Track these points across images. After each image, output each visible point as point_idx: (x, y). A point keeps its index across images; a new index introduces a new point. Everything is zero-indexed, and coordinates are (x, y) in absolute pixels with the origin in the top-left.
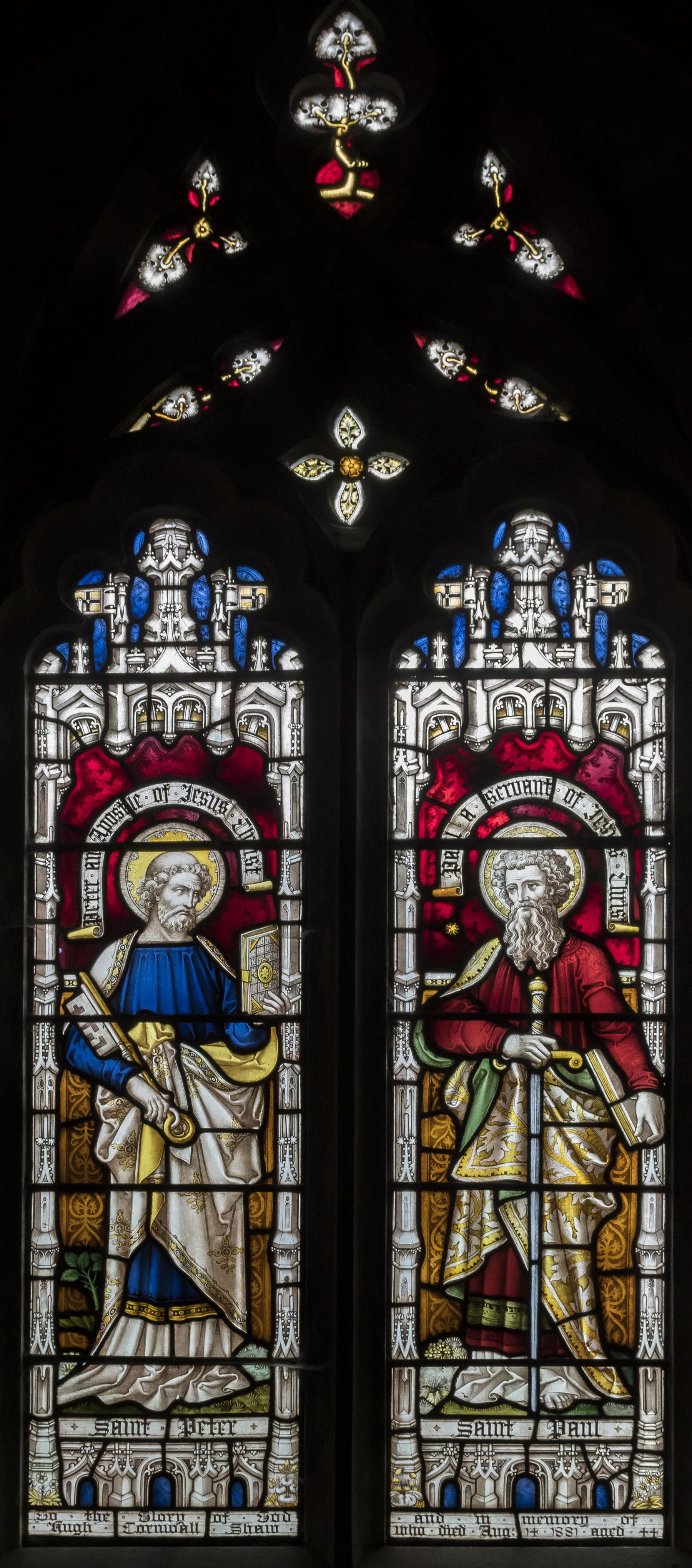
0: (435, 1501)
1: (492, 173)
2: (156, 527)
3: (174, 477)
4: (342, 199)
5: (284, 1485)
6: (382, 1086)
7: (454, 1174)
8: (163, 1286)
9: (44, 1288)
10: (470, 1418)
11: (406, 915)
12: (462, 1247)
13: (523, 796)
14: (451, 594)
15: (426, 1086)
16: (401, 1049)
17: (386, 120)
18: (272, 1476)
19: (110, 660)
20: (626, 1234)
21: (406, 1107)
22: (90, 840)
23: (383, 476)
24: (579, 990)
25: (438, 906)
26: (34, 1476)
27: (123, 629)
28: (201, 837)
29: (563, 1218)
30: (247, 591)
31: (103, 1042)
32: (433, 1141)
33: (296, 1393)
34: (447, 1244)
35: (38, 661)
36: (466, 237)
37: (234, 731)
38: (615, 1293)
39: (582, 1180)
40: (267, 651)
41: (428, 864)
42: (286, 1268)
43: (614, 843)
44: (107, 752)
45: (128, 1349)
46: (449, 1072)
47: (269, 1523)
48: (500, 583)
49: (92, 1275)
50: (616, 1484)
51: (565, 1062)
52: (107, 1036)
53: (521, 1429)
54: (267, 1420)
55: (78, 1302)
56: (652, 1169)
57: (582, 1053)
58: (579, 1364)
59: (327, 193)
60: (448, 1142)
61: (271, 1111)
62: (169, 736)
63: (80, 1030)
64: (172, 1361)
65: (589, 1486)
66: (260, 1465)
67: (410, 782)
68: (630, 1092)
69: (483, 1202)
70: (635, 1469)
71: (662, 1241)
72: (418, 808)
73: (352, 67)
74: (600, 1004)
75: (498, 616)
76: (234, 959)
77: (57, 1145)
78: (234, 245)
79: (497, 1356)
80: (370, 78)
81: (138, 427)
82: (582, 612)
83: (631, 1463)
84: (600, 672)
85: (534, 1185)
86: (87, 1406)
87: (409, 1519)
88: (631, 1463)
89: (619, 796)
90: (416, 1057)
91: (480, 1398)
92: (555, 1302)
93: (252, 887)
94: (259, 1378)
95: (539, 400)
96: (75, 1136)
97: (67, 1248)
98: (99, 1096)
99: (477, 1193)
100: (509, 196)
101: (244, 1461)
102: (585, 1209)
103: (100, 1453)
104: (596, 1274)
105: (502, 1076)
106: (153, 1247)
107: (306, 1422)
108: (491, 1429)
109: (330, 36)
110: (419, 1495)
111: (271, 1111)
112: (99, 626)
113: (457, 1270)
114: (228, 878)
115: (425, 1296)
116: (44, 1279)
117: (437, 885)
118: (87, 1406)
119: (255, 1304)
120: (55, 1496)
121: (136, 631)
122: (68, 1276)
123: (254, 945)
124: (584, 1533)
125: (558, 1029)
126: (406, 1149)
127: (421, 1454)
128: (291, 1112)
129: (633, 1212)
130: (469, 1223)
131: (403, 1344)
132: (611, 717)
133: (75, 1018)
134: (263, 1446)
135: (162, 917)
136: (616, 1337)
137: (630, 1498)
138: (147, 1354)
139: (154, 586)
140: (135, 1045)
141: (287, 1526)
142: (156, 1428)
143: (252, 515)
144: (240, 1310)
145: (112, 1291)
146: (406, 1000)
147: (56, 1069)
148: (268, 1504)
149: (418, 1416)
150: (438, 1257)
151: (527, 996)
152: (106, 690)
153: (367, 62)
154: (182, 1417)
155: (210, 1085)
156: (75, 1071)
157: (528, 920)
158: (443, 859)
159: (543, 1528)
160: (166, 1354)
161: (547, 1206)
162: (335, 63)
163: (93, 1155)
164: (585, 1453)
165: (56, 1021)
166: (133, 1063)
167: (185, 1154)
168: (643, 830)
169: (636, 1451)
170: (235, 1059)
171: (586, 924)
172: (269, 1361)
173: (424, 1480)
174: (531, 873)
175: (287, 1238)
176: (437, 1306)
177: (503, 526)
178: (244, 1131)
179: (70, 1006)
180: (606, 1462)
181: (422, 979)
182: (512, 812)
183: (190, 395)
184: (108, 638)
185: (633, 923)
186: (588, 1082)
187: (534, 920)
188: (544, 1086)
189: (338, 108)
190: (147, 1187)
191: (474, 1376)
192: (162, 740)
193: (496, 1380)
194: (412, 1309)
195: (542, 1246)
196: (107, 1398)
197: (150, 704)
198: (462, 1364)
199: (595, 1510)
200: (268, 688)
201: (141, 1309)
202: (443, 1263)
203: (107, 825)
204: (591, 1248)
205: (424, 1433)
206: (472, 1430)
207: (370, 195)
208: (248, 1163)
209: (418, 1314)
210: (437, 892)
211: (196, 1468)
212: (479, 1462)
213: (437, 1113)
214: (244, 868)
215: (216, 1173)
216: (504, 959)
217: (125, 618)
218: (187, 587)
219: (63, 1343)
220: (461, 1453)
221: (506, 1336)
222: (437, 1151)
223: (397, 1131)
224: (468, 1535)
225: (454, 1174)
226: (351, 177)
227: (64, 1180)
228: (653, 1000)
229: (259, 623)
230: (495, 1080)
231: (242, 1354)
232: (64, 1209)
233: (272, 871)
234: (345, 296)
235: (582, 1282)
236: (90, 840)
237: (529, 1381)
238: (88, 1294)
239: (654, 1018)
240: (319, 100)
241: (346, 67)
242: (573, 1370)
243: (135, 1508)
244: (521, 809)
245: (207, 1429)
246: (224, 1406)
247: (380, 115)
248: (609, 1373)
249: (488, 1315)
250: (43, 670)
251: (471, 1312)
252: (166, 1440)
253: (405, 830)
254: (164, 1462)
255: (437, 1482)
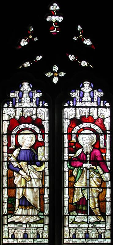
0: (72, 237)
1: (79, 28)
2: (23, 83)
3: (27, 75)
4: (54, 32)
5: (46, 235)
6: (62, 172)
7: (74, 186)
8: (25, 203)
9: (6, 204)
10: (78, 224)
11: (66, 145)
12: (76, 197)
13: (86, 126)
14: (73, 95)
15: (70, 172)
16: (65, 166)
17: (61, 20)
18: (44, 233)
19: (16, 105)
20: (104, 195)
21: (66, 175)
22: (13, 133)
23: (61, 76)
24: (95, 157)
25: (71, 143)
26: (4, 234)
27: (18, 100)
28: (31, 132)
29: (93, 192)
30: (39, 94)
31: (15, 165)
32: (71, 180)
33: (48, 220)
34: (73, 197)
35: (4, 104)
36: (75, 39)
37: (37, 116)
38: (102, 204)
39: (96, 187)
40: (42, 103)
41: (70, 137)
42: (46, 200)
43: (101, 134)
44: (16, 119)
45: (20, 213)
46: (73, 170)
47: (44, 241)
48: (81, 93)
49: (14, 201)
50: (102, 234)
51: (93, 168)
52: (16, 164)
53: (86, 226)
54: (43, 224)
55: (11, 206)
56: (108, 185)
57: (96, 167)
58: (96, 215)
59: (51, 31)
60: (73, 181)
61: (44, 176)
62: (26, 117)
63: (11, 163)
64: (27, 215)
65: (98, 235)
66: (42, 232)
67: (66, 124)
68: (104, 173)
69: (79, 190)
70: (106, 232)
71: (110, 196)
72: (68, 128)
73: (55, 11)
74: (99, 159)
75: (81, 98)
76: (37, 152)
77: (8, 181)
78: (36, 39)
79: (82, 214)
80: (59, 13)
81: (20, 68)
82: (95, 97)
83: (105, 231)
84: (99, 107)
85: (88, 187)
86: (13, 222)
87: (67, 240)
88: (105, 231)
89: (103, 127)
90: (68, 167)
91: (79, 221)
92: (92, 206)
93: (40, 140)
94: (42, 218)
95: (88, 64)
96: (11, 180)
97: (9, 198)
98: (15, 173)
99: (78, 189)
100: (82, 32)
101: (39, 231)
102: (97, 191)
103: (15, 230)
104: (99, 201)
105: (82, 171)
106: (24, 197)
107: (49, 225)
108: (81, 226)
109: (52, 7)
110: (69, 236)
111: (44, 176)
112: (14, 99)
113: (75, 201)
114: (36, 139)
115: (70, 205)
116: (6, 202)
117: (71, 140)
118: (13, 222)
119: (41, 206)
120: (7, 236)
121: (20, 100)
122: (10, 202)
123: (40, 150)
124: (97, 242)
125: (92, 163)
126: (66, 182)
127: (69, 230)
128: (47, 176)
129: (105, 191)
130: (77, 193)
131: (66, 212)
132: (101, 114)
133: (10, 161)
134: (42, 229)
135: (25, 145)
136: (102, 211)
137: (105, 236)
138: (23, 214)
139: (23, 93)
140: (20, 165)
141: (47, 241)
142: (25, 226)
143: (39, 83)
144: (39, 207)
145: (17, 204)
146: (66, 158)
147: (7, 169)
148: (43, 238)
149: (69, 224)
150: (72, 199)
151: (87, 158)
152: (15, 109)
153: (58, 11)
154: (29, 224)
155: (33, 172)
156: (11, 169)
157: (87, 146)
158: (72, 136)
159: (90, 241)
160: (26, 214)
161: (90, 191)
162: (53, 11)
163: (14, 183)
164: (97, 230)
165: (7, 161)
166: (20, 168)
167: (29, 182)
168: (106, 132)
169: (106, 229)
170: (37, 168)
171: (97, 146)
172: (44, 215)
173: (70, 234)
174: (88, 138)
175: (46, 195)
176: (72, 206)
177: (82, 84)
178: (39, 179)
179: (10, 159)
180: (101, 231)
181: (69, 155)
182: (84, 129)
183: (29, 63)
184: (15, 101)
185: (105, 146)
186: (97, 171)
187: (88, 146)
188: (90, 172)
189: (53, 18)
190: (23, 188)
191: (78, 217)
192: (25, 117)
193: (82, 218)
194: (68, 207)
195: (90, 197)
196: (16, 221)
197: (22, 112)
198: (76, 216)
199: (99, 238)
200: (42, 109)
201: (22, 207)
202: (73, 200)
203: (15, 131)
204: (98, 197)
205: (70, 227)
206: (78, 226)
207: (58, 32)
208: (40, 184)
209: (68, 208)
210: (71, 141)
211: (31, 232)
212: (79, 231)
213: (71, 176)
214: (38, 137)
215: (34, 186)
216: (83, 152)
217: (18, 98)
218: (29, 93)
219: (9, 213)
220: (76, 230)
221: (84, 211)
222: (71, 182)
223: (65, 179)
224: (77, 242)
225: (74, 186)
226: (56, 29)
227: (9, 187)
228: (108, 158)
229: (41, 99)
230: (81, 171)
231: (39, 214)
232: (9, 191)
233: (43, 138)
234: (55, 47)
235: (96, 203)
236: (13, 133)
237: (88, 218)
238: (13, 205)
239: (108, 161)
240: (50, 16)
241: (55, 11)
242: (95, 216)
243: (21, 239)
244: (85, 128)
245: (33, 226)
246: (36, 222)
247: (60, 19)
248: (101, 217)
249: (80, 208)
250: (4, 106)
251: (77, 207)
252: (26, 228)
253: (66, 131)
254: (26, 231)
255: (72, 234)
